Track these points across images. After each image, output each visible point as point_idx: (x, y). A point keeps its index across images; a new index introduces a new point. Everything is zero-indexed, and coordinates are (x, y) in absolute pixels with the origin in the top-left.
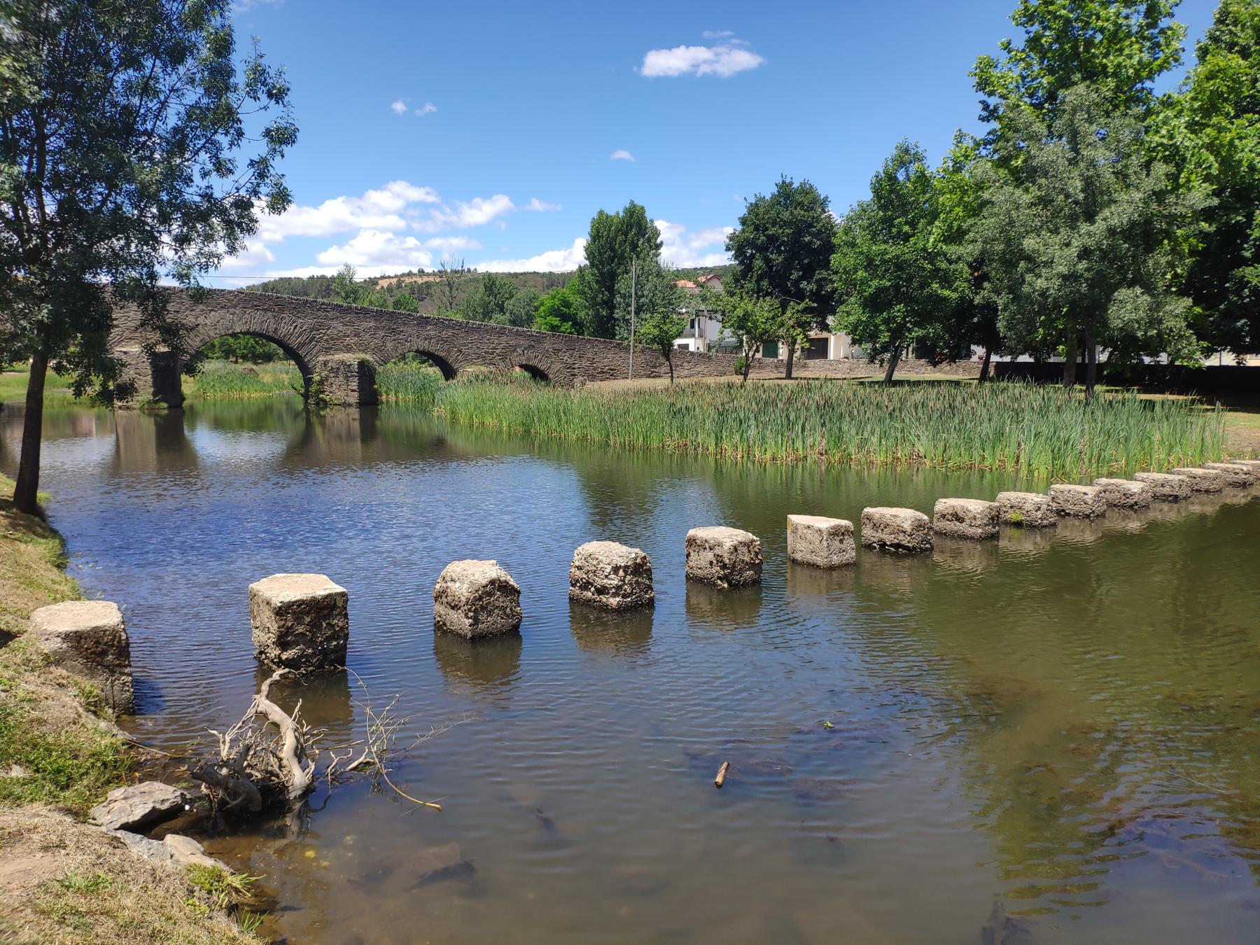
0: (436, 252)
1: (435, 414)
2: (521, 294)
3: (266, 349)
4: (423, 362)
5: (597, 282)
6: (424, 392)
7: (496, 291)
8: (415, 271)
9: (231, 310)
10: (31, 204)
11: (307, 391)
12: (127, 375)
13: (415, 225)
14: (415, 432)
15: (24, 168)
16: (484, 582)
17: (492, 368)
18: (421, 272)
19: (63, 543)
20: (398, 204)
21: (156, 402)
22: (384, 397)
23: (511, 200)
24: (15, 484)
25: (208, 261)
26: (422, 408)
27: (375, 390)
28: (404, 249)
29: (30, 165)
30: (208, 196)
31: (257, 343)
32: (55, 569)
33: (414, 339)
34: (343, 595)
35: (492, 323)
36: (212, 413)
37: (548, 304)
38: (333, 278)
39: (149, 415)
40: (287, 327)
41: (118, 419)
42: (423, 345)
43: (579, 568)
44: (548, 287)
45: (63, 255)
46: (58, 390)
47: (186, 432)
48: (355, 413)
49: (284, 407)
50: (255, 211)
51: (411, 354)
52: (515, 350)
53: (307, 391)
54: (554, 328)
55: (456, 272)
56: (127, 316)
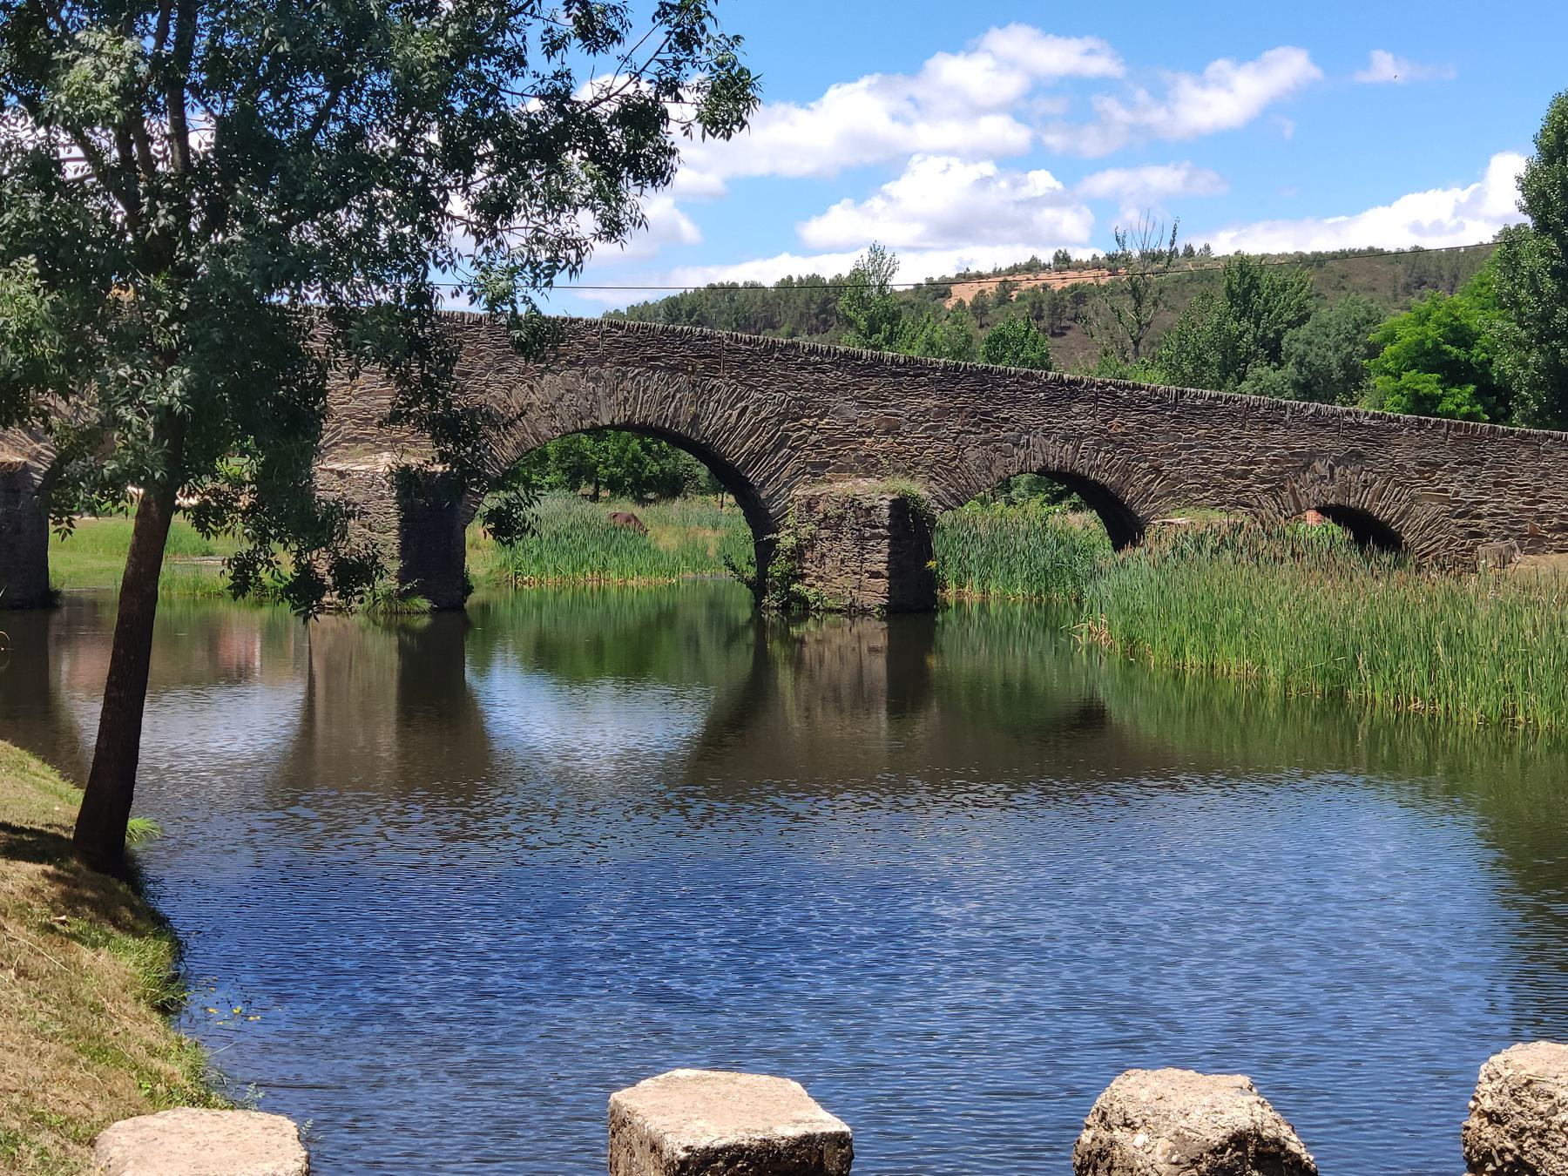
0: (1104, 207)
1: (1083, 641)
2: (1332, 312)
3: (669, 465)
4: (1056, 499)
5: (1555, 273)
6: (1058, 573)
7: (1258, 303)
8: (1046, 257)
9: (592, 370)
10: (158, 126)
11: (762, 573)
12: (356, 539)
13: (1054, 140)
14: (1027, 686)
15: (150, 43)
16: (1216, 1138)
17: (1242, 516)
18: (1063, 261)
19: (179, 950)
20: (1011, 86)
21: (404, 596)
22: (952, 591)
23: (1315, 59)
24: (79, 795)
25: (561, 257)
26: (1049, 620)
27: (931, 574)
28: (1018, 203)
29: (161, 37)
30: (558, 97)
31: (646, 448)
32: (156, 1017)
33: (1036, 439)
34: (840, 1140)
35: (1246, 392)
36: (533, 626)
37: (1408, 336)
38: (838, 286)
39: (388, 628)
40: (729, 412)
41: (316, 637)
42: (1057, 454)
43: (1494, 1118)
44: (1407, 289)
45: (223, 250)
46: (197, 562)
47: (469, 675)
48: (875, 633)
49: (701, 615)
50: (673, 133)
51: (1025, 478)
52: (1307, 467)
53: (762, 573)
54: (1422, 404)
55: (1156, 257)
56: (358, 392)
